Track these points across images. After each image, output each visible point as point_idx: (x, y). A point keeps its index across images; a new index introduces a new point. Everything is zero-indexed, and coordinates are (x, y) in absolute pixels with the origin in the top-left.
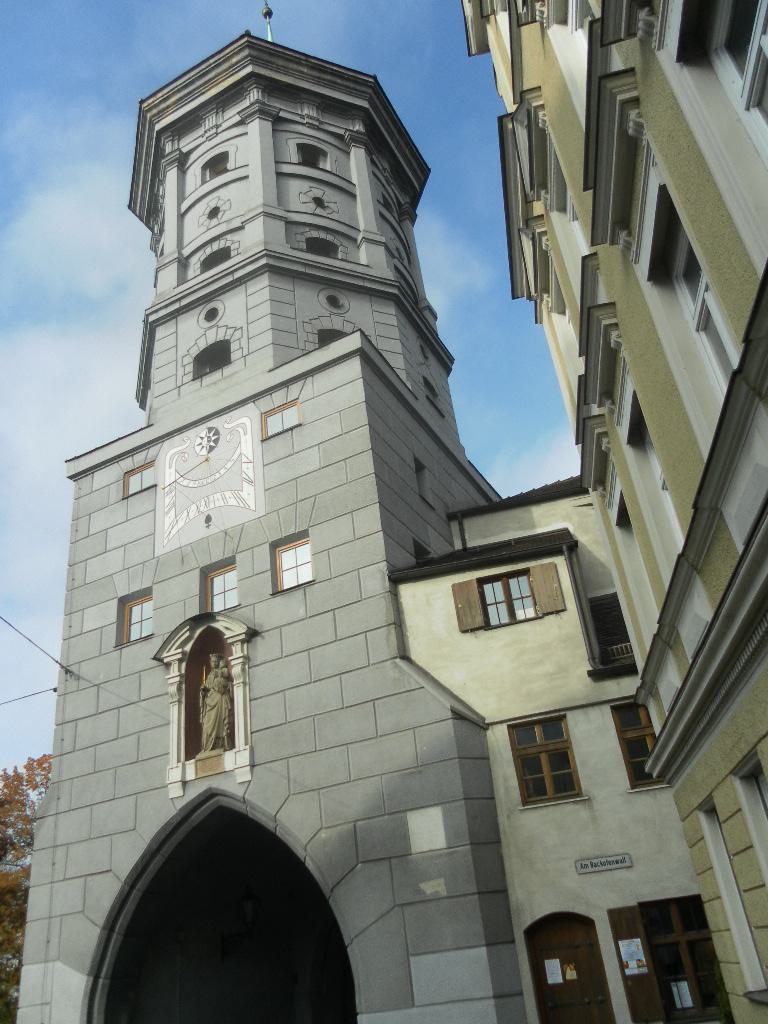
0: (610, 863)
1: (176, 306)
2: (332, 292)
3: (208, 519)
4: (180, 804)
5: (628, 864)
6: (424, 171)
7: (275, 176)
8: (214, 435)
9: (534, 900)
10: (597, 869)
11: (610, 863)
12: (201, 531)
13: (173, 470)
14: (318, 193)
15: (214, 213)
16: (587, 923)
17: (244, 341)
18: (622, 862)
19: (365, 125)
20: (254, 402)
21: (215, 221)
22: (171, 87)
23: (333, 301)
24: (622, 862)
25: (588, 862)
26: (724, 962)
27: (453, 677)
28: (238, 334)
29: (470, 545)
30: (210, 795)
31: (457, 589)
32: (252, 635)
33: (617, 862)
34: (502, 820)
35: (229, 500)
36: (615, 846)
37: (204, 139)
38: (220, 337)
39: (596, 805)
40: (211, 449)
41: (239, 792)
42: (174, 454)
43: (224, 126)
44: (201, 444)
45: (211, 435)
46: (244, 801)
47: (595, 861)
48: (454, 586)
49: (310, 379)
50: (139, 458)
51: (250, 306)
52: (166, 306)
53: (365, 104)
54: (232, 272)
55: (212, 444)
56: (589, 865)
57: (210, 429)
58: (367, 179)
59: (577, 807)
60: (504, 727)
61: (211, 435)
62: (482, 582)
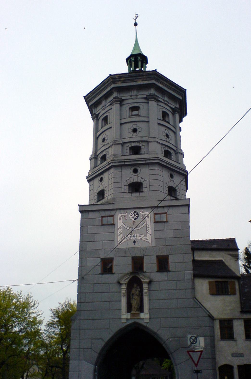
1: (123, 163)
2: (172, 173)
3: (134, 242)
4: (125, 325)
5: (243, 356)
9: (222, 361)
12: (131, 245)
13: (121, 221)
14: (167, 132)
15: (135, 130)
17: (148, 185)
18: (242, 355)
19: (179, 106)
20: (151, 208)
23: (172, 176)
24: (242, 355)
25: (234, 354)
28: (145, 182)
30: (135, 323)
32: (150, 283)
34: (216, 342)
35: (139, 236)
36: (241, 351)
37: (131, 98)
38: (139, 181)
39: (237, 342)
40: (135, 219)
41: (145, 324)
42: (122, 216)
43: (139, 97)
44: (132, 216)
45: (136, 214)
47: (236, 354)
50: (107, 213)
52: (119, 162)
54: (145, 160)
55: (136, 217)
56: (235, 355)
57: (135, 212)
58: (177, 128)
59: (233, 342)
61: (136, 214)
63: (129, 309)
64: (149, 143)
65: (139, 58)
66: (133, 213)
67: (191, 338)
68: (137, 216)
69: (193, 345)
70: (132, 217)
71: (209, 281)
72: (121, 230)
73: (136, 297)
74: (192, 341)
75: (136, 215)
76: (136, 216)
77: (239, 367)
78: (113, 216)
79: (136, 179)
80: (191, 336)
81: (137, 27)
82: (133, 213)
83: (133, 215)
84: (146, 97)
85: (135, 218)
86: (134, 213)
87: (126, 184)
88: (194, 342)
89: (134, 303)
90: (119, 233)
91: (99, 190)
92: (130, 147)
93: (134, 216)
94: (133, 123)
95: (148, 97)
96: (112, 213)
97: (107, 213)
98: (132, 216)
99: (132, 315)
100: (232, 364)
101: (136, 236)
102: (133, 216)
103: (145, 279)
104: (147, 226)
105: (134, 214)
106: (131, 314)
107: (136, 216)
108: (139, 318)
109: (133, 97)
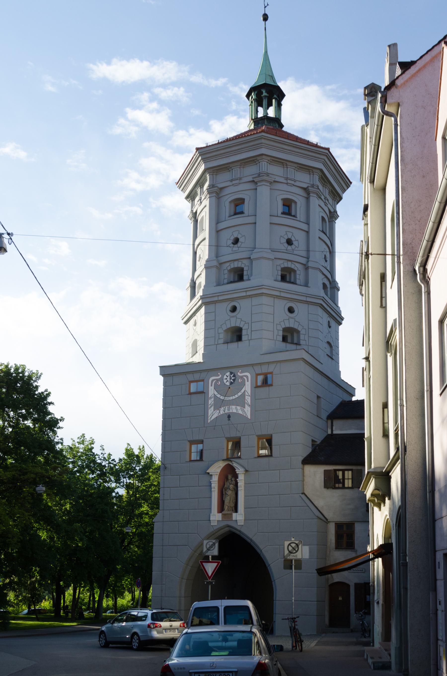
0: (358, 570)
4: (215, 528)
5: (364, 571)
6: (342, 319)
7: (269, 224)
8: (233, 377)
10: (354, 571)
11: (358, 570)
16: (348, 586)
17: (249, 331)
21: (235, 248)
22: (217, 158)
26: (288, 636)
27: (320, 503)
29: (335, 432)
31: (325, 471)
33: (361, 570)
35: (235, 408)
44: (226, 379)
45: (232, 376)
46: (261, 551)
48: (325, 471)
49: (279, 364)
50: (197, 376)
51: (233, 236)
53: (320, 166)
55: (232, 381)
60: (334, 524)
61: (232, 376)
62: (335, 471)
63: (221, 509)
64: (253, 261)
65: (265, 94)
66: (228, 374)
67: (289, 544)
68: (234, 379)
69: (292, 554)
70: (227, 381)
71: (323, 470)
72: (212, 401)
73: (229, 492)
74: (290, 548)
75: (233, 378)
76: (233, 380)
77: (356, 585)
78: (203, 380)
79: (234, 323)
80: (290, 542)
81: (266, 22)
82: (228, 375)
83: (229, 377)
84: (252, 179)
85: (231, 382)
86: (229, 375)
87: (221, 331)
88: (295, 551)
89: (228, 501)
90: (210, 405)
91: (193, 340)
92: (228, 269)
93: (229, 379)
94: (233, 229)
95: (256, 180)
96: (203, 375)
97: (197, 376)
98: (226, 379)
99: (224, 516)
100: (347, 582)
101: (231, 408)
102: (228, 379)
103: (240, 469)
104: (246, 394)
105: (230, 377)
106: (222, 514)
107: (233, 380)
108: (232, 519)
109: (234, 182)
